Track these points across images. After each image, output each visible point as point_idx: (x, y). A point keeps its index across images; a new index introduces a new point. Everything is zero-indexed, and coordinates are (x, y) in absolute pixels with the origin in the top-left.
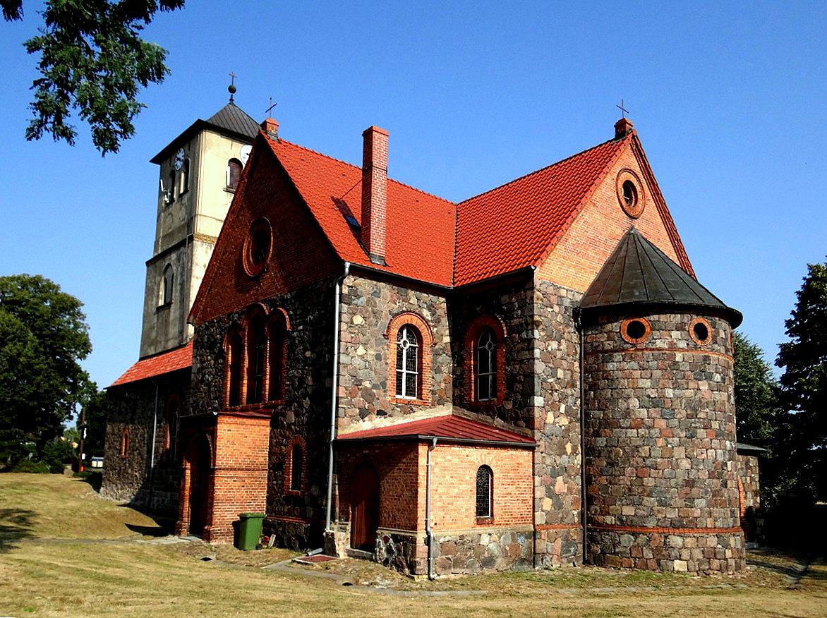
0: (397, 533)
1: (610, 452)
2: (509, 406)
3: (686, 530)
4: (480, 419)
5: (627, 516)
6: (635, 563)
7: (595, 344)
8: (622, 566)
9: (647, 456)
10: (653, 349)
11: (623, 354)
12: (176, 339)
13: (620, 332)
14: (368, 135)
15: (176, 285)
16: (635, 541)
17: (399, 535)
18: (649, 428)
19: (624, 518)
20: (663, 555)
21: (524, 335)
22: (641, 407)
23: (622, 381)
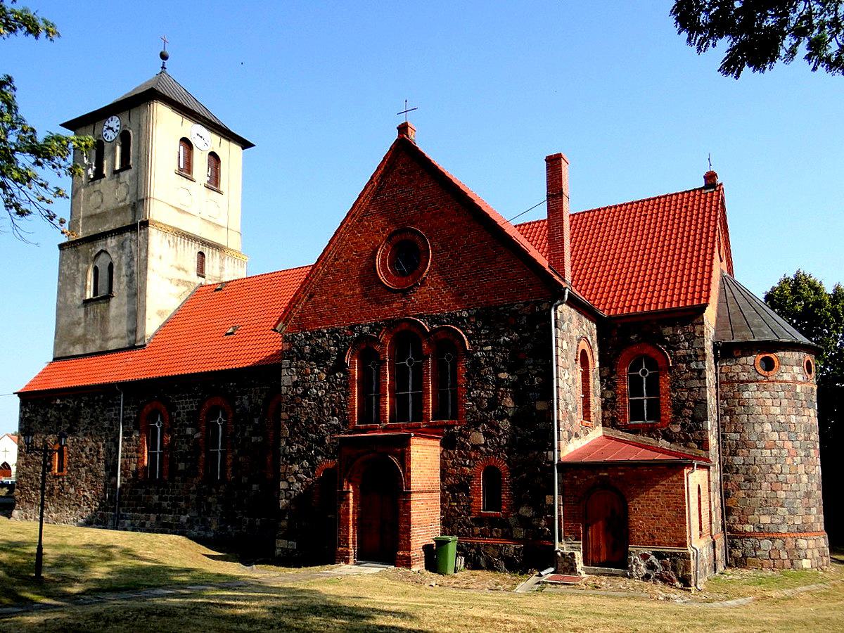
0: (661, 550)
2: (676, 429)
4: (640, 441)
6: (774, 564)
7: (730, 375)
8: (763, 567)
10: (782, 382)
12: (123, 338)
13: (754, 365)
14: (554, 164)
15: (119, 277)
16: (773, 545)
17: (664, 552)
18: (780, 449)
20: (795, 555)
21: (693, 365)
22: (773, 431)
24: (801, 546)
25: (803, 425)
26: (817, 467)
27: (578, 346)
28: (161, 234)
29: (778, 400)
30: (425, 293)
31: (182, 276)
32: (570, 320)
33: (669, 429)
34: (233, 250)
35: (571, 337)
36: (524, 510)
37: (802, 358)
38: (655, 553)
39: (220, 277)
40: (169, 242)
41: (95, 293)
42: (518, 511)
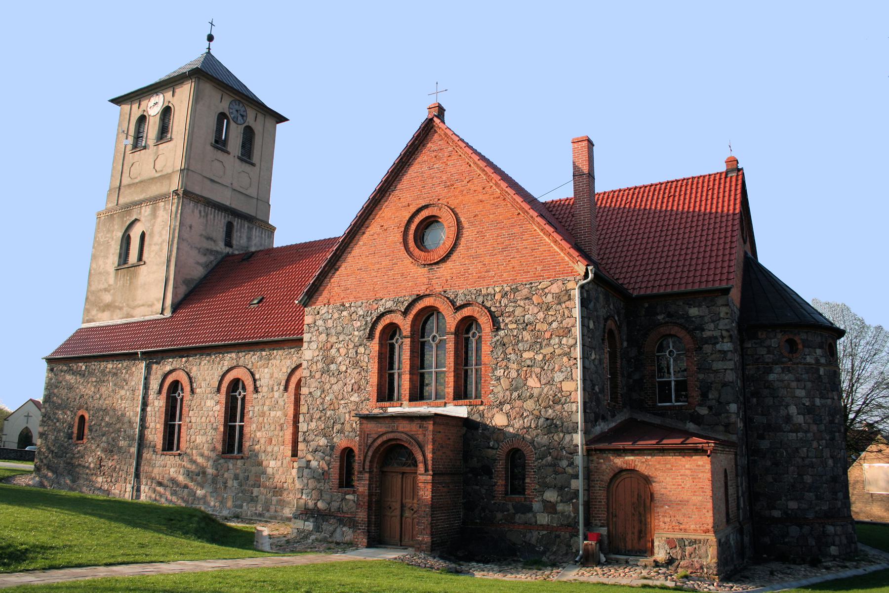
5: (792, 510)
7: (756, 357)
9: (805, 456)
11: (782, 366)
22: (798, 414)
25: (827, 409)
26: (842, 451)
27: (605, 325)
31: (210, 245)
32: (597, 299)
35: (598, 317)
36: (548, 495)
39: (247, 248)
40: (200, 212)
42: (542, 495)
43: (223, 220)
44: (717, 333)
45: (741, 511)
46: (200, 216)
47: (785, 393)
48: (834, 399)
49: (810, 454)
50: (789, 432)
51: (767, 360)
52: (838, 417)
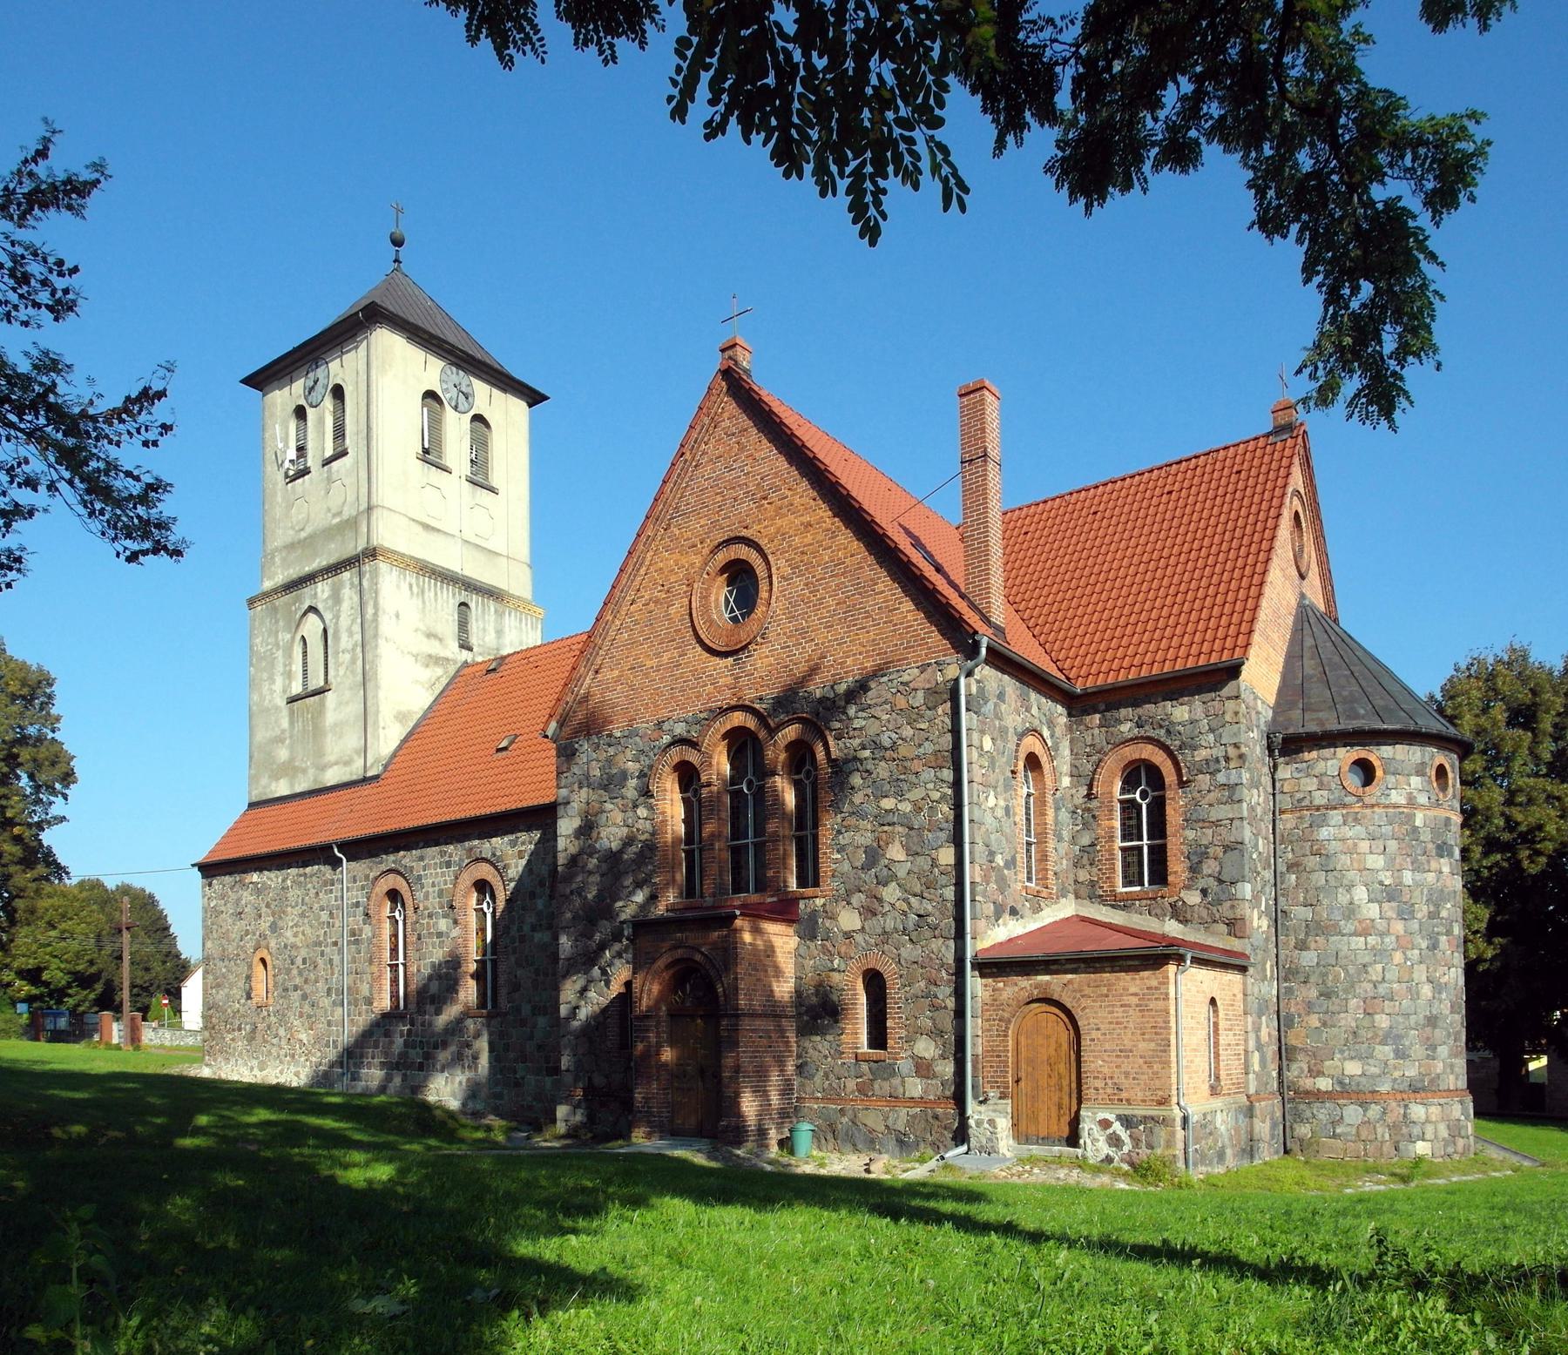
1: (1325, 975)
3: (1429, 1095)
5: (1351, 1077)
6: (1365, 1150)
7: (1299, 796)
10: (1386, 807)
18: (1382, 935)
19: (1347, 1081)
21: (1221, 778)
23: (1343, 857)
24: (1414, 1117)
25: (1425, 891)
26: (1453, 970)
27: (1018, 745)
28: (395, 572)
29: (1380, 843)
30: (767, 657)
31: (434, 648)
32: (1001, 696)
33: (1181, 899)
34: (519, 598)
37: (1427, 759)
38: (1119, 1118)
39: (498, 649)
40: (411, 586)
41: (305, 684)
43: (451, 601)
44: (1218, 752)
45: (1251, 1076)
46: (412, 594)
47: (1349, 862)
48: (1441, 872)
49: (1388, 976)
50: (1351, 935)
51: (1317, 802)
52: (1449, 906)
